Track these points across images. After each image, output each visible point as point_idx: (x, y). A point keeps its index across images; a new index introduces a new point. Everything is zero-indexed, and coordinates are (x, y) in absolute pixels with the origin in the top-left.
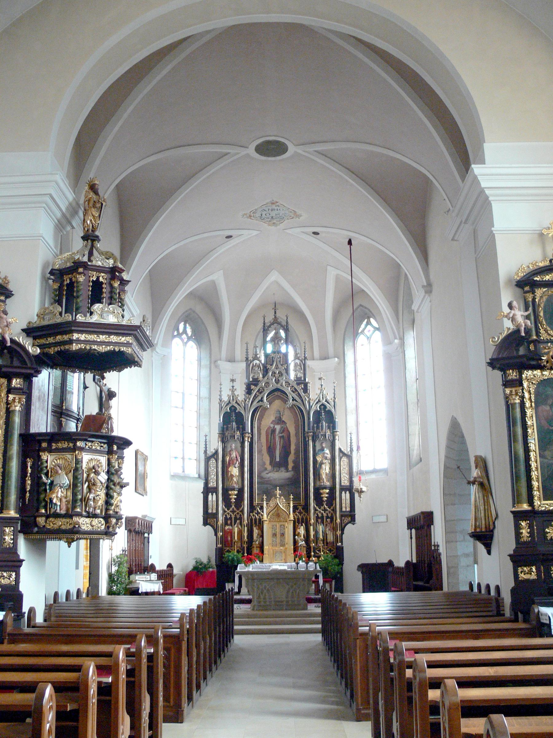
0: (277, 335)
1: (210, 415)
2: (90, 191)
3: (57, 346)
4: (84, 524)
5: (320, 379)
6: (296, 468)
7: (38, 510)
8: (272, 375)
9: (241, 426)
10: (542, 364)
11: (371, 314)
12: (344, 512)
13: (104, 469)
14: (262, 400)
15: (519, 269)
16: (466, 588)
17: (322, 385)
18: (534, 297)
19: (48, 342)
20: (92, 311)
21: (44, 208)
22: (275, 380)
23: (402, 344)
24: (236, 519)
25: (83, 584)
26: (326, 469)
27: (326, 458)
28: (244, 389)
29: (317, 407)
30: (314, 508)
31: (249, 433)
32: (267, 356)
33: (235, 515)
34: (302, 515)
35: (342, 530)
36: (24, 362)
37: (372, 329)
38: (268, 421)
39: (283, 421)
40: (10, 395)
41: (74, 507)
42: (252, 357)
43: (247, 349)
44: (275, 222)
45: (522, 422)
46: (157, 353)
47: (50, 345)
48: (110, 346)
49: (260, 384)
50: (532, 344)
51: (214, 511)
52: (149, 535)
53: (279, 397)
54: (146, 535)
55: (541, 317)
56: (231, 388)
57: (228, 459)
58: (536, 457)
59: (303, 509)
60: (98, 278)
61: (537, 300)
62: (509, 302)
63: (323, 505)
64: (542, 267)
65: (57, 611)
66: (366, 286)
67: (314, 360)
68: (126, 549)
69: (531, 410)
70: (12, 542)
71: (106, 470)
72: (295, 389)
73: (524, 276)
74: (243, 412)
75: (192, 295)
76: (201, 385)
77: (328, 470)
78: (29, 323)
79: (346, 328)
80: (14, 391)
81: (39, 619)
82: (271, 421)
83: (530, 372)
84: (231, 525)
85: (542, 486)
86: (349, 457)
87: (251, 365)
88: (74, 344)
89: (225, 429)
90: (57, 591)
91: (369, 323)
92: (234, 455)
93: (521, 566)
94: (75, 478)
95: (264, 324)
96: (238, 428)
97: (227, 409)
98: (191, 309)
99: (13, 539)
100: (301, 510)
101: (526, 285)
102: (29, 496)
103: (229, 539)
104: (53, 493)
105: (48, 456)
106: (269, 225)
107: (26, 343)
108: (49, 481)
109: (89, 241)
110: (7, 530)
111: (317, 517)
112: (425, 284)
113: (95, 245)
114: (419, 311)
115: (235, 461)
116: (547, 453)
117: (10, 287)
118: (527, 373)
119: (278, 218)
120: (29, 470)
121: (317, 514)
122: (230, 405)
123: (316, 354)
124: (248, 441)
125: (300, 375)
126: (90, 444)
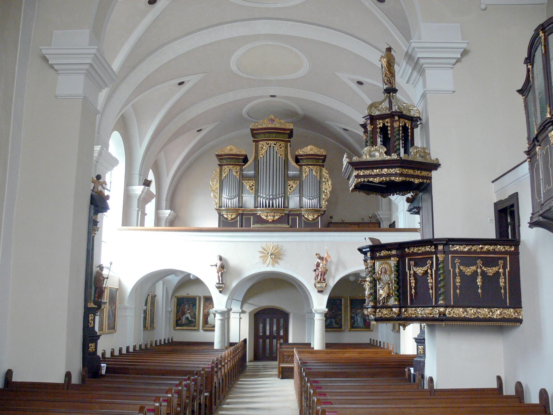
45: (385, 258)
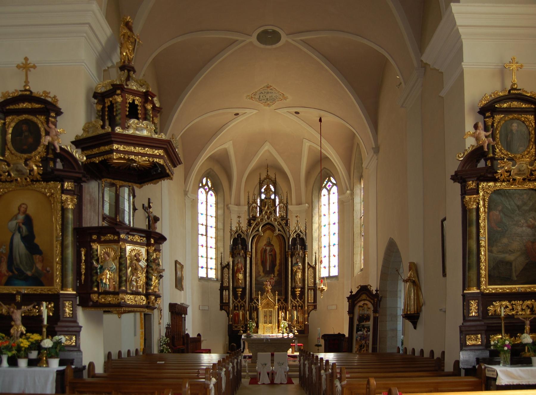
0: (268, 190)
1: (224, 240)
2: (125, 27)
3: (100, 156)
4: (129, 300)
5: (297, 217)
6: (279, 275)
7: (92, 288)
8: (265, 214)
9: (244, 247)
10: (497, 177)
11: (331, 174)
12: (310, 303)
13: (144, 257)
14: (258, 230)
15: (483, 97)
16: (395, 351)
17: (298, 221)
18: (493, 122)
19: (93, 153)
21: (85, 38)
23: (352, 194)
24: (241, 306)
25: (140, 346)
26: (299, 275)
27: (299, 268)
28: (247, 223)
29: (294, 236)
30: (291, 300)
31: (249, 252)
32: (262, 201)
33: (241, 304)
34: (283, 304)
35: (309, 314)
37: (331, 184)
38: (262, 244)
40: (63, 195)
41: (120, 287)
42: (252, 202)
43: (249, 196)
44: (269, 103)
46: (189, 197)
47: (95, 156)
48: (145, 157)
49: (257, 220)
50: (489, 161)
51: (227, 302)
52: (185, 315)
53: (269, 229)
54: (183, 316)
55: (498, 138)
56: (238, 222)
57: (236, 268)
58: (485, 251)
59: (284, 301)
60: (134, 101)
61: (495, 125)
62: (474, 123)
63: (296, 298)
64: (502, 96)
65: (113, 364)
66: (329, 154)
67: (292, 205)
68: (170, 324)
69: (484, 214)
70: (71, 312)
71: (146, 258)
72: (280, 223)
73: (487, 103)
74: (246, 238)
75: (212, 158)
76: (218, 220)
77: (300, 277)
78: (77, 136)
79: (314, 184)
81: (99, 369)
82: (264, 244)
83: (485, 184)
84: (238, 310)
85: (488, 274)
86: (314, 268)
88: (115, 154)
89: (234, 249)
90: (443, 350)
91: (329, 180)
92: (240, 266)
93: (469, 334)
94: (120, 264)
95: (260, 179)
96: (242, 249)
97: (235, 236)
98: (210, 169)
99: (72, 311)
101: (487, 111)
102: (85, 278)
104: (103, 275)
105: (98, 246)
106: (265, 105)
107: (73, 152)
108: (99, 266)
109: (126, 71)
111: (293, 306)
112: (374, 147)
113: (131, 75)
114: (368, 168)
115: (240, 270)
116: (494, 249)
117: (60, 105)
118: (483, 184)
119: (271, 99)
120: (84, 258)
121: (293, 304)
122: (237, 233)
123: (294, 201)
124: (249, 257)
125: (284, 214)
126: (132, 237)
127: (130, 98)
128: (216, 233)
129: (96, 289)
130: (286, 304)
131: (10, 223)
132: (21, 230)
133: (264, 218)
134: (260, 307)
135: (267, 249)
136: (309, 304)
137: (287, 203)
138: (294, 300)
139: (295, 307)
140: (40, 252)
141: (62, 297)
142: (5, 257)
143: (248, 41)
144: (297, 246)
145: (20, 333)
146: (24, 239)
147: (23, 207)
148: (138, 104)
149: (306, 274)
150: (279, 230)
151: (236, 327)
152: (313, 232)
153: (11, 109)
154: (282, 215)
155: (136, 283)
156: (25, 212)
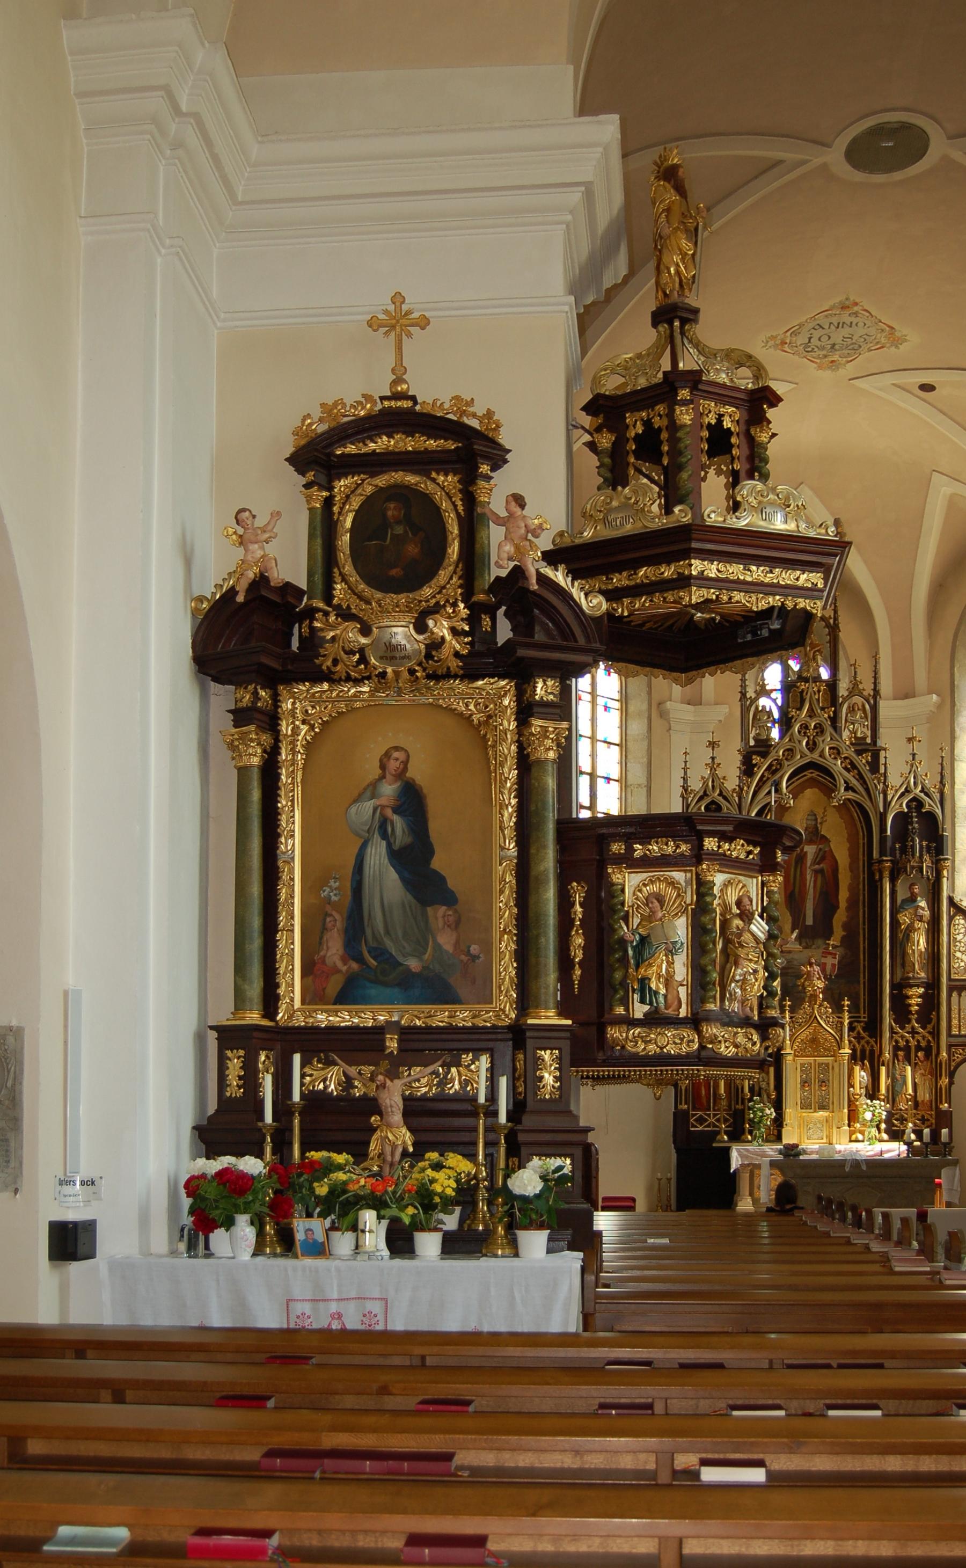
5: (910, 740)
6: (849, 941)
8: (799, 732)
12: (955, 1036)
17: (914, 755)
20: (739, 498)
22: (807, 743)
26: (921, 942)
28: (738, 764)
29: (901, 805)
30: (891, 1028)
34: (863, 1042)
35: (951, 1075)
36: (565, 632)
39: (823, 837)
42: (755, 692)
44: (836, 358)
49: (773, 753)
53: (813, 783)
59: (864, 1029)
63: (909, 1021)
72: (852, 763)
80: (540, 710)
87: (753, 709)
100: (861, 1032)
103: (703, 1092)
106: (820, 367)
110: (546, 1055)
111: (896, 1048)
117: (504, 439)
121: (897, 1042)
122: (707, 800)
125: (863, 731)
127: (710, 412)
128: (621, 799)
129: (620, 1010)
130: (872, 1041)
131: (353, 810)
132: (389, 829)
133: (797, 745)
134: (788, 1051)
135: (806, 853)
136: (953, 1040)
137: (876, 692)
138: (902, 1028)
139: (904, 1052)
140: (449, 899)
141: (531, 1038)
142: (337, 916)
143: (817, 161)
144: (913, 840)
145: (400, 1150)
146: (397, 857)
147: (397, 759)
148: (733, 429)
149: (945, 938)
150: (848, 788)
151: (701, 1120)
152: (956, 793)
153: (350, 455)
154: (859, 735)
155: (741, 990)
156: (401, 774)
